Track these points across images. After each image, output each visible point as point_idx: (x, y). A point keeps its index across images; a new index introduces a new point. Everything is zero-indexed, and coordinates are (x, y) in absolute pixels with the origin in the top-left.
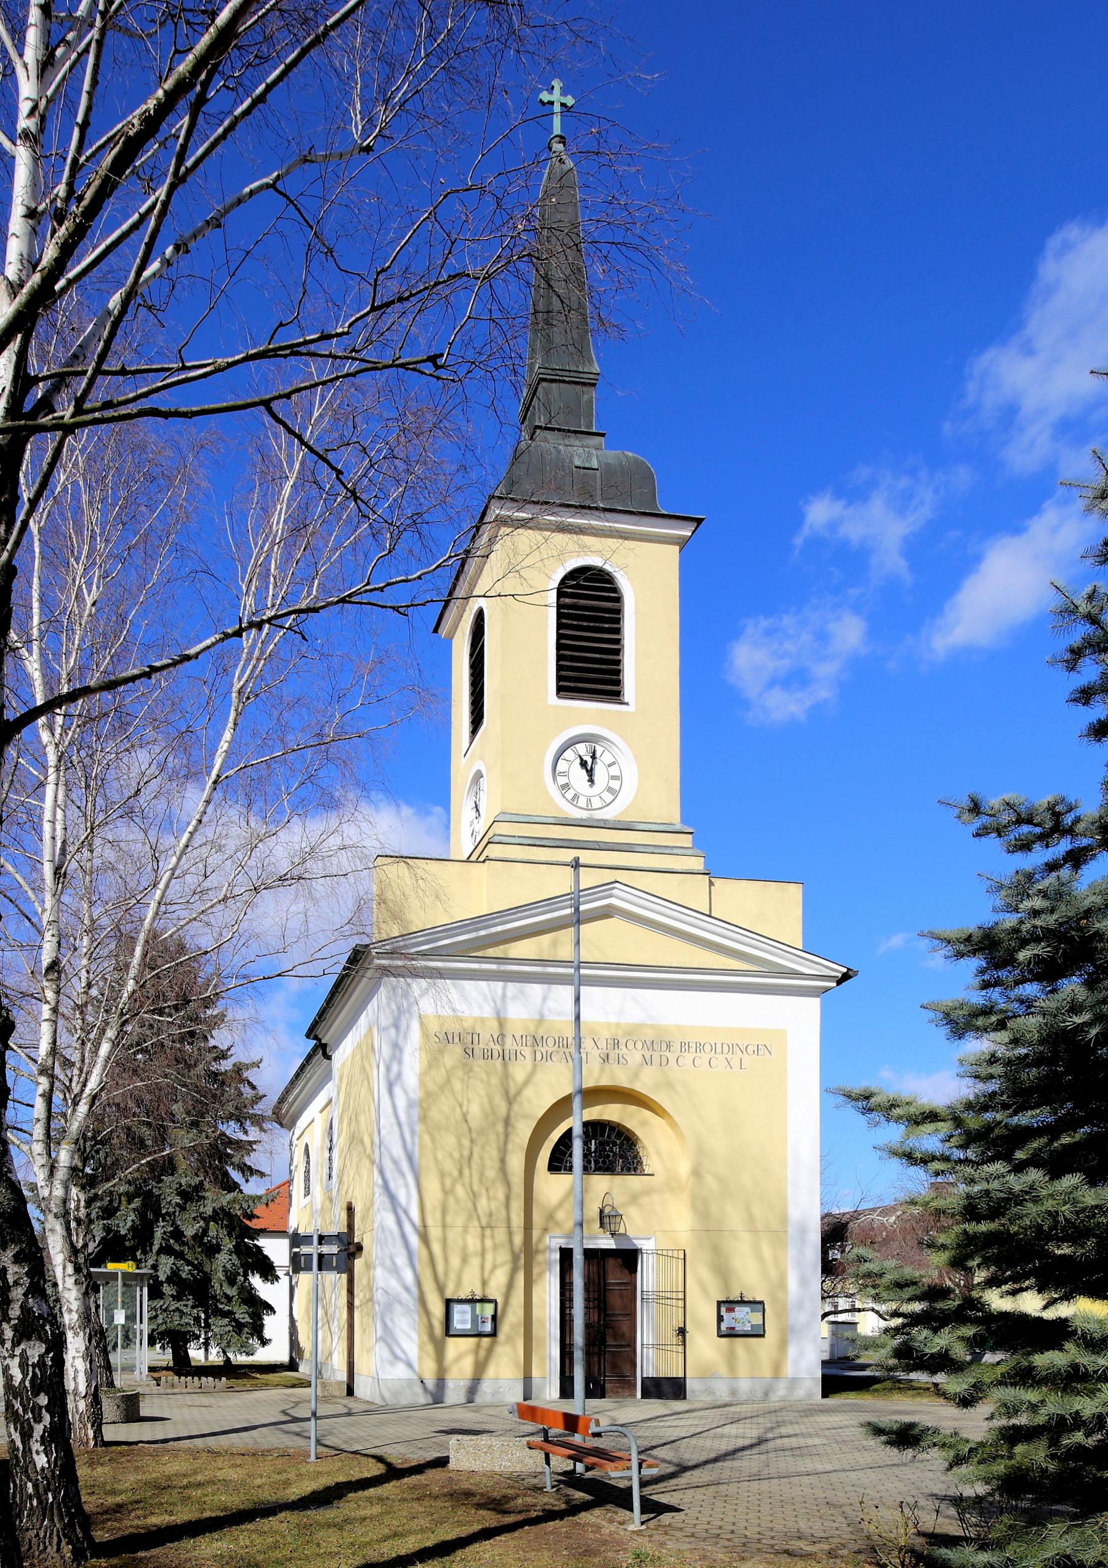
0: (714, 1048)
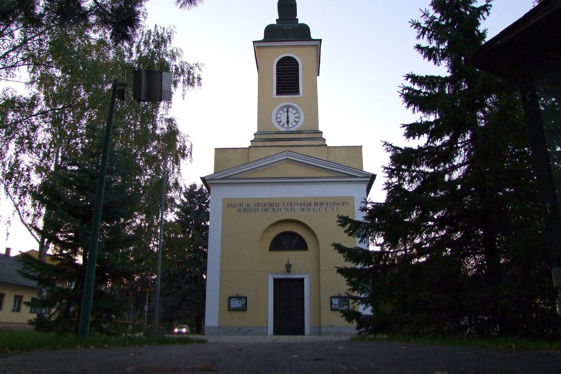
0: (327, 204)
